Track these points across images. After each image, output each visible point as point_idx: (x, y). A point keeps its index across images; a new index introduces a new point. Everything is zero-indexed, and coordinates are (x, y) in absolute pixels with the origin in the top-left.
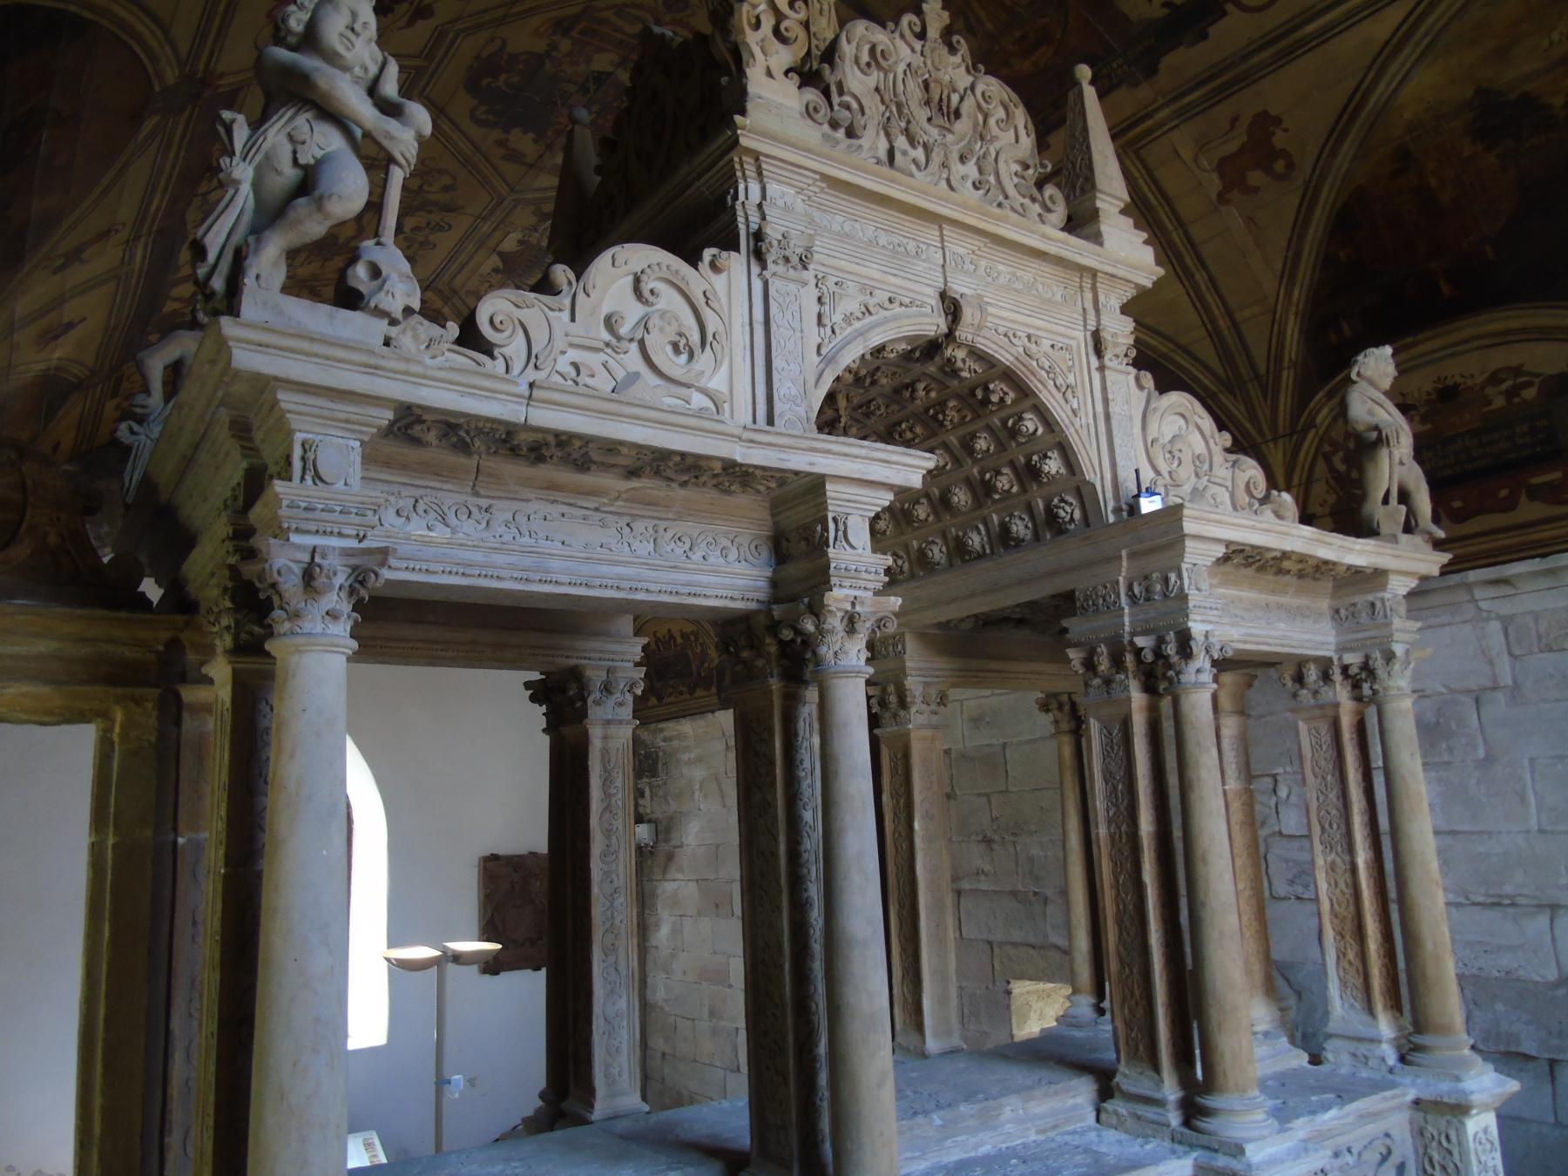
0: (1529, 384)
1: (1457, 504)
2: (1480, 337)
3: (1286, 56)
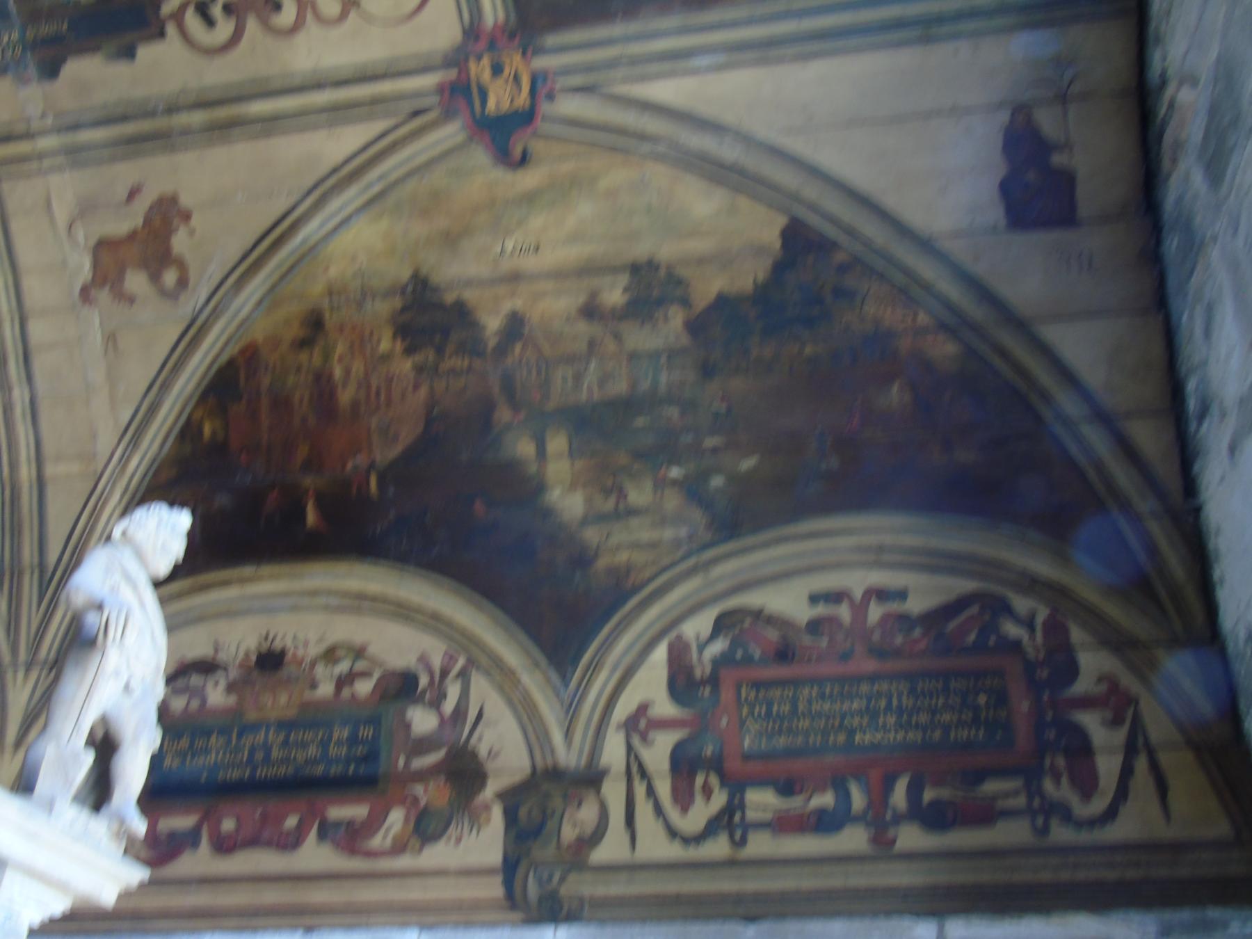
0: (365, 674)
1: (228, 825)
3: (222, 131)
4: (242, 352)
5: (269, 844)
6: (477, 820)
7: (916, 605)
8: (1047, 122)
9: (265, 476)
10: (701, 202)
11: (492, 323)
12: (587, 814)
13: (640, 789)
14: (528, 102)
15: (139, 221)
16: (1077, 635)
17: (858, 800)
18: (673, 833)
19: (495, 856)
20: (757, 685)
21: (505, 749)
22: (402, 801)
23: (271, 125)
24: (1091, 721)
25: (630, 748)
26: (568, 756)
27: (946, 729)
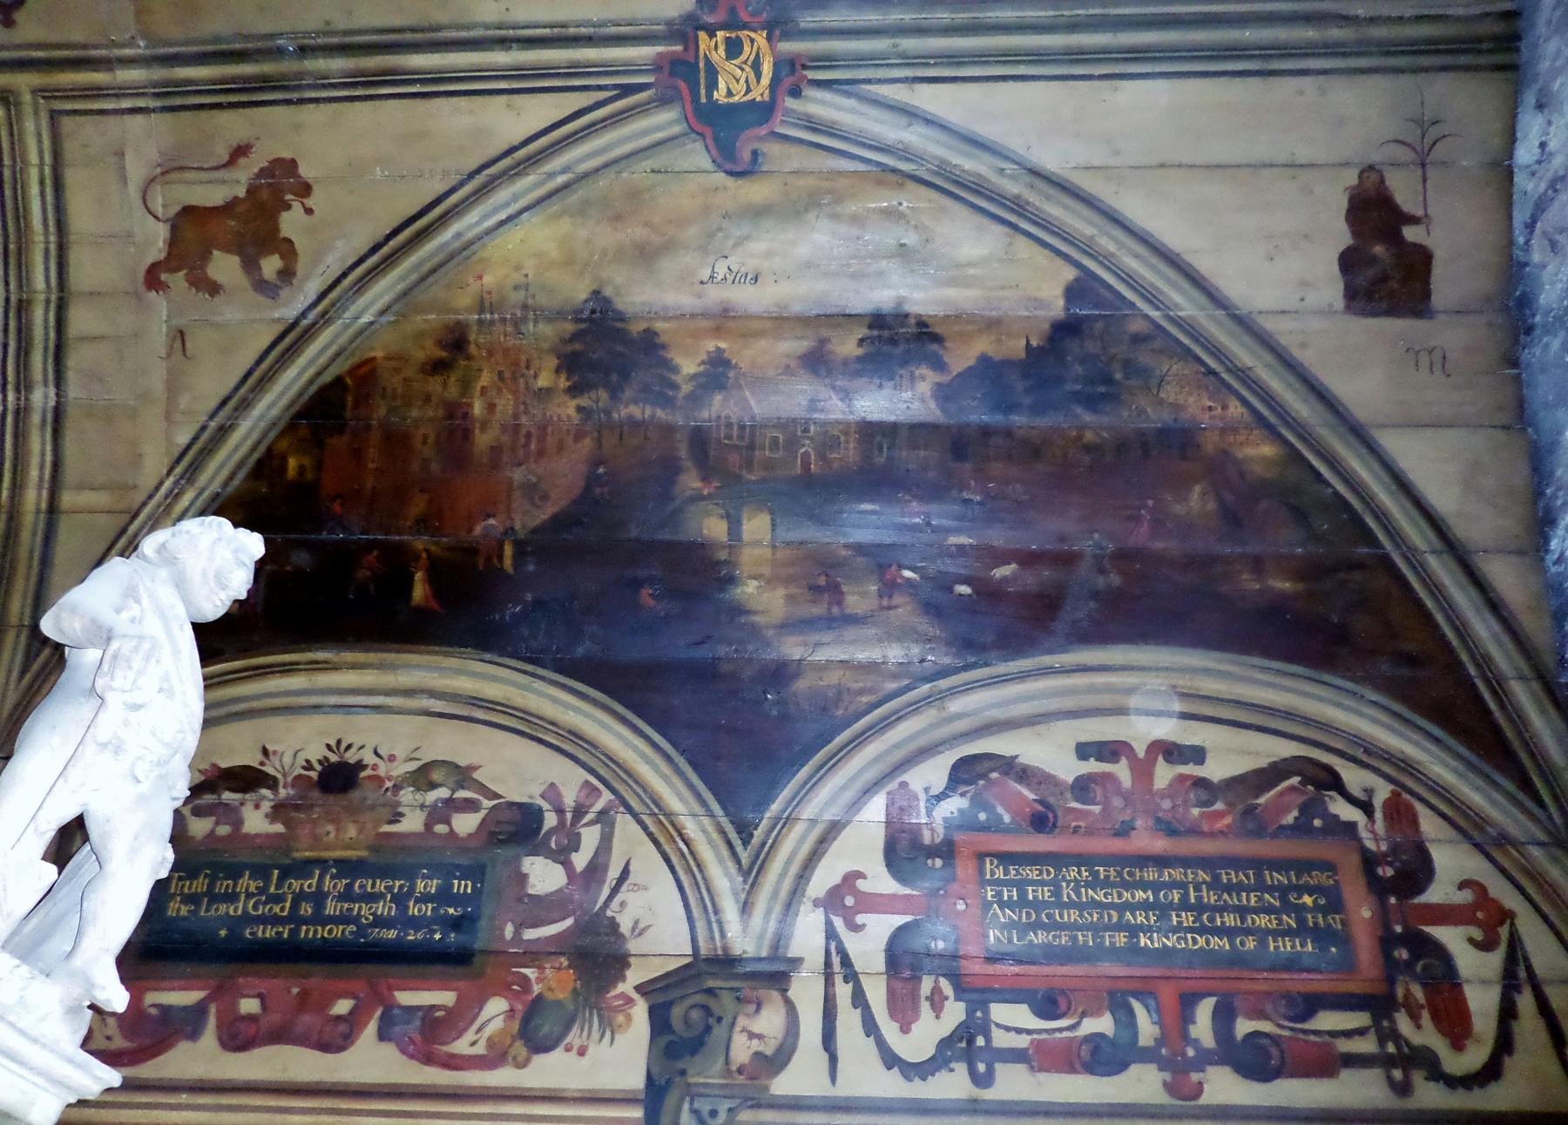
0: (470, 806)
1: (249, 1006)
2: (432, 694)
3: (367, 87)
4: (352, 371)
5: (302, 1041)
6: (609, 1027)
7: (1216, 770)
8: (1403, 190)
9: (365, 535)
10: (970, 241)
11: (689, 366)
12: (769, 1022)
13: (843, 991)
14: (766, 97)
15: (241, 192)
16: (1429, 825)
17: (1147, 1028)
18: (890, 1060)
19: (635, 1080)
20: (1006, 858)
21: (657, 923)
22: (503, 989)
23: (435, 86)
24: (1451, 937)
25: (831, 934)
26: (744, 937)
27: (1262, 935)
